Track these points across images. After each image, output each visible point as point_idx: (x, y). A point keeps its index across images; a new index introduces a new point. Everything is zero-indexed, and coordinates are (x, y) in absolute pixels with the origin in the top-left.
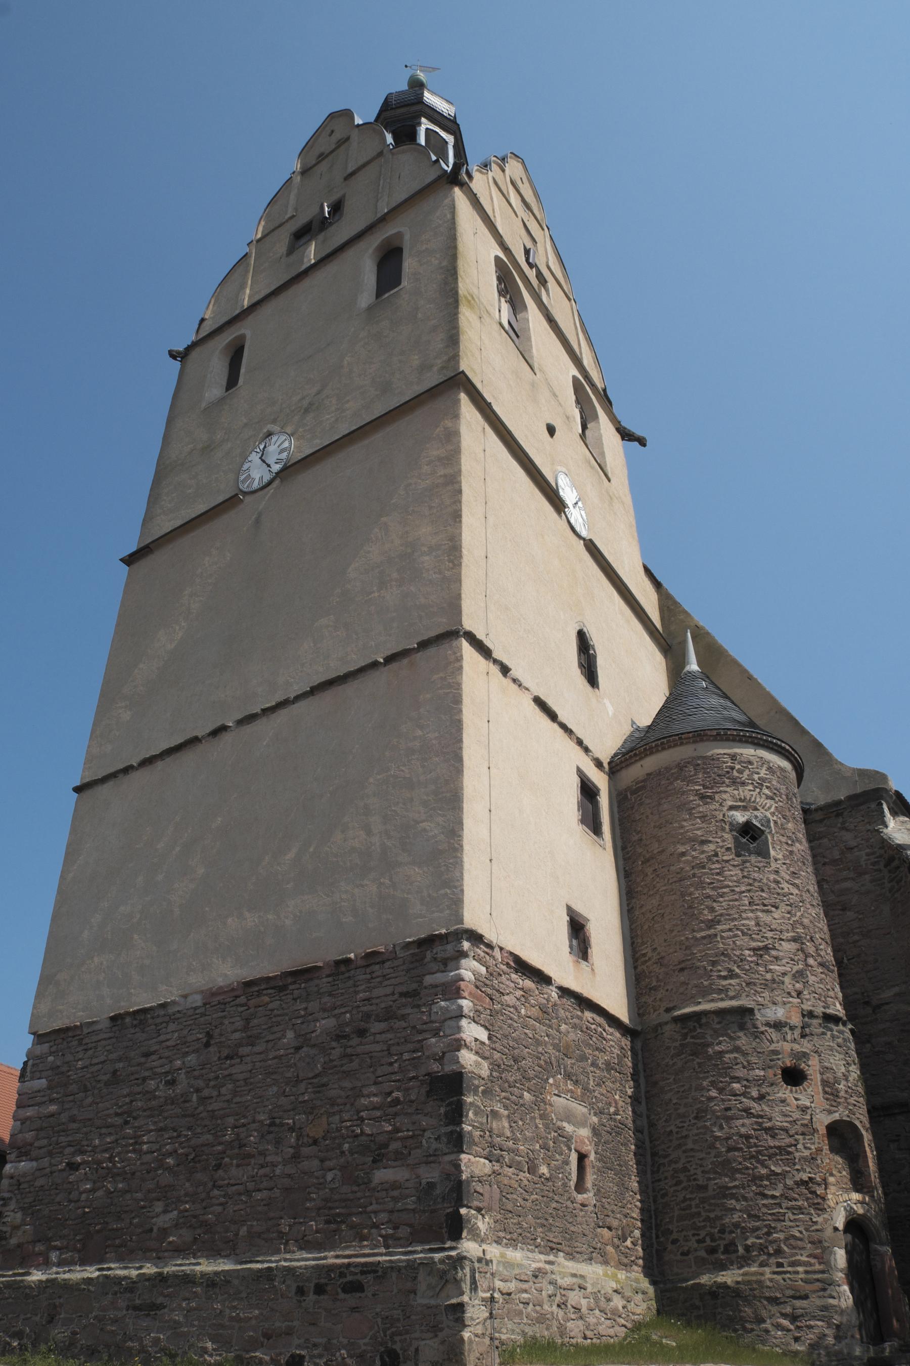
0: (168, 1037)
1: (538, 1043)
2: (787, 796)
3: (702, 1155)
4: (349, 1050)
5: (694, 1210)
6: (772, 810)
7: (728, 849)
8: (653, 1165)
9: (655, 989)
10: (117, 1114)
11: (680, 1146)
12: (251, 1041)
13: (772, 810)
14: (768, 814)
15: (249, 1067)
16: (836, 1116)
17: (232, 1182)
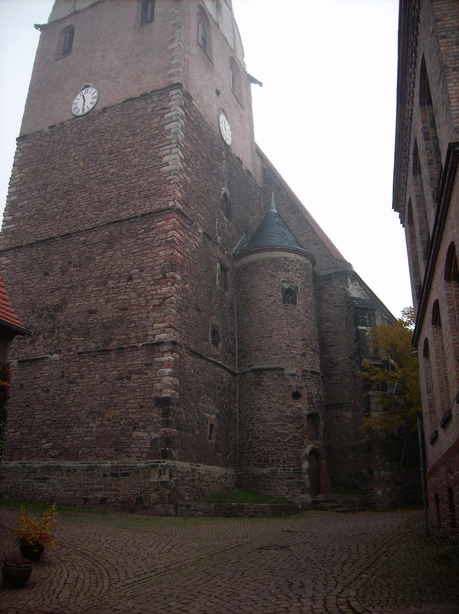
0: (45, 372)
1: (197, 383)
2: (307, 276)
3: (258, 425)
4: (123, 385)
5: (254, 446)
6: (300, 283)
7: (280, 300)
8: (239, 427)
9: (246, 356)
10: (23, 402)
11: (250, 421)
12: (82, 377)
13: (300, 283)
14: (298, 285)
15: (81, 388)
16: (311, 411)
17: (75, 433)
